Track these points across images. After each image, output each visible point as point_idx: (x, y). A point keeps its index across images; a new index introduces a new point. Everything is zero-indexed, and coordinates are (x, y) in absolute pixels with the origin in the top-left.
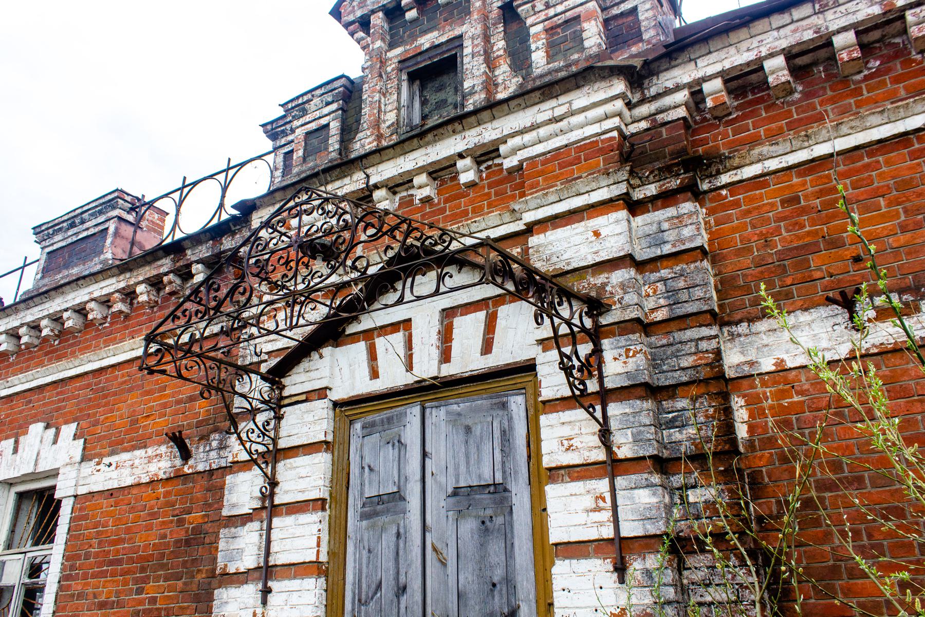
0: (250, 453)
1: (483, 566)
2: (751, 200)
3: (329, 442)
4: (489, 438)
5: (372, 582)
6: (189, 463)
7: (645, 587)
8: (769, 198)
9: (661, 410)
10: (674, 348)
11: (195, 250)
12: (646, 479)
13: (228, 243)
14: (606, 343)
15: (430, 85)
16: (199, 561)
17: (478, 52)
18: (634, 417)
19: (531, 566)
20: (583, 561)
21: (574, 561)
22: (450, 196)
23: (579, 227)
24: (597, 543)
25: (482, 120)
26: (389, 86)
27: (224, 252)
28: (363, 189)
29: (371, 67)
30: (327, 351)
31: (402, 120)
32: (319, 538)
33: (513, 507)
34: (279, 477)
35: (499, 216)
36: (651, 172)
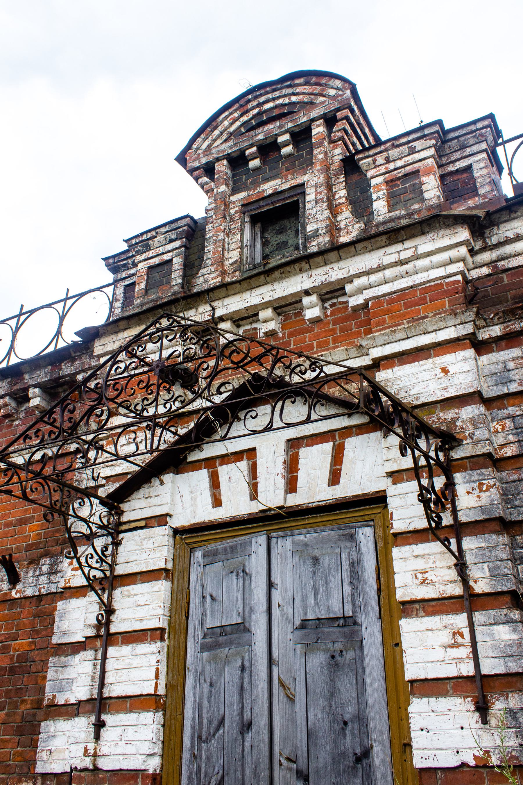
0: (88, 578)
1: (333, 703)
3: (169, 570)
4: (338, 570)
5: (214, 717)
6: (17, 587)
7: (509, 728)
9: (515, 545)
11: (33, 374)
12: (506, 615)
13: (67, 369)
14: (458, 477)
15: (271, 228)
16: (24, 690)
17: (322, 199)
18: (490, 551)
19: (384, 704)
20: (442, 699)
21: (433, 700)
22: (294, 331)
23: (427, 364)
24: (454, 681)
25: (328, 260)
26: (232, 227)
27: (63, 377)
28: (208, 321)
29: (216, 209)
30: (168, 478)
31: (245, 258)
32: (157, 669)
33: (364, 641)
34: (116, 605)
35: (345, 351)
36: (496, 315)
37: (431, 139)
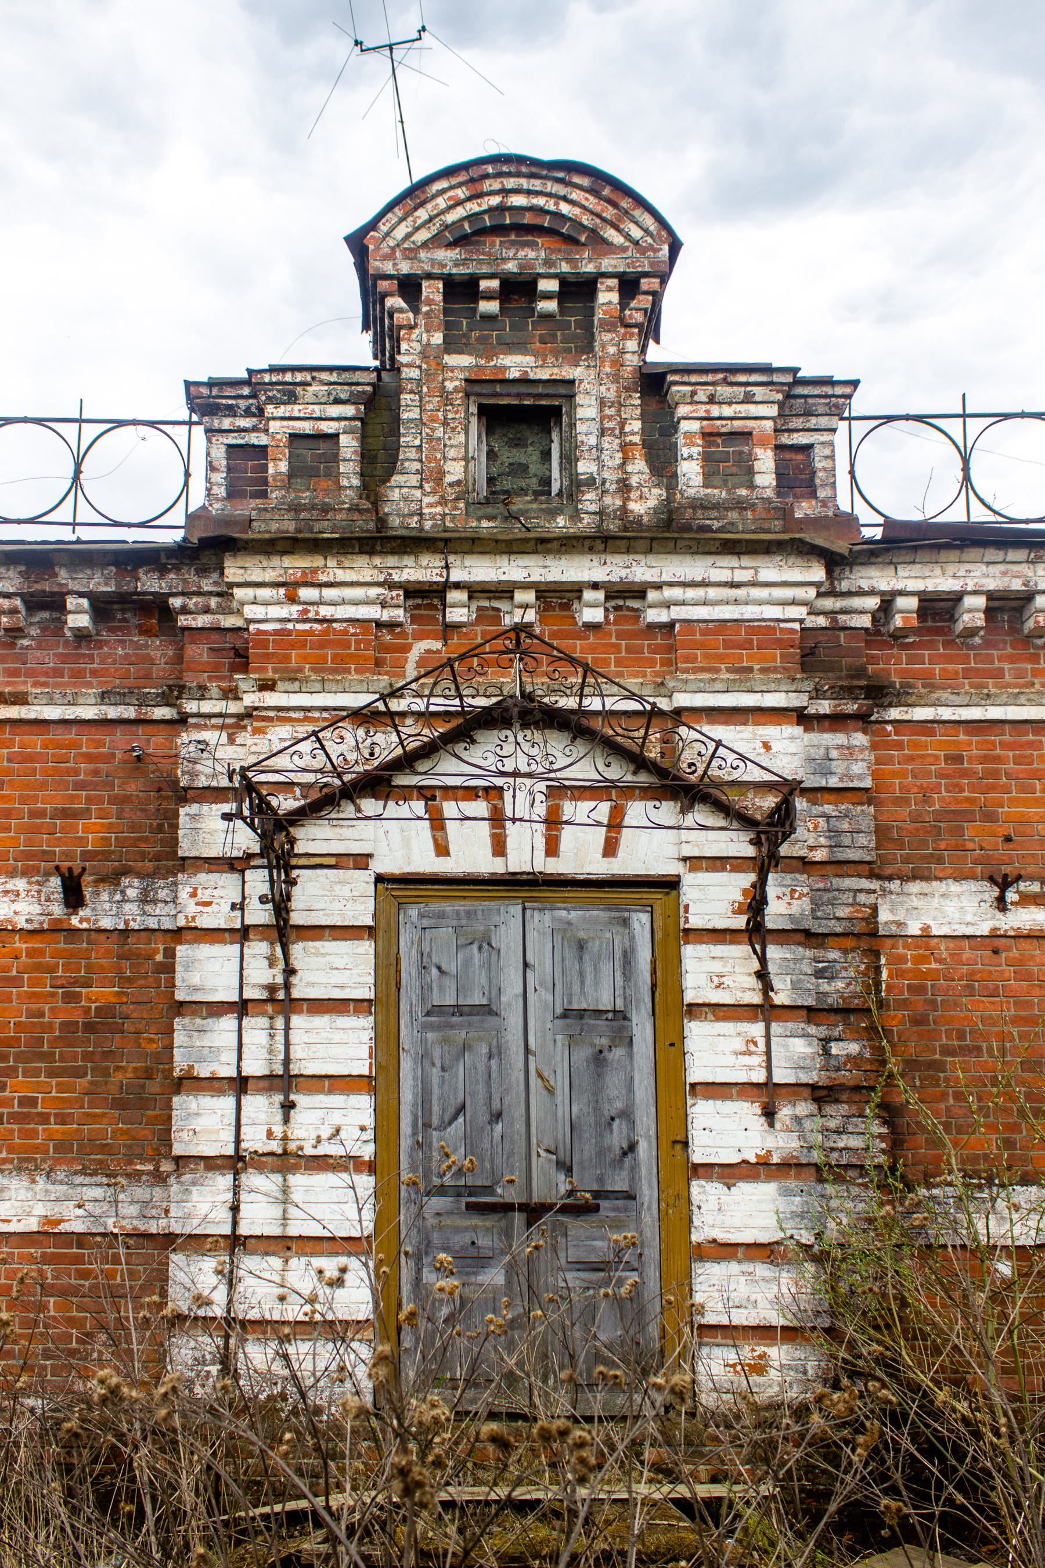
2: (916, 745)
6: (81, 913)
8: (934, 748)
10: (831, 895)
17: (613, 429)
21: (719, 1103)
26: (450, 416)
34: (296, 964)
37: (778, 392)
